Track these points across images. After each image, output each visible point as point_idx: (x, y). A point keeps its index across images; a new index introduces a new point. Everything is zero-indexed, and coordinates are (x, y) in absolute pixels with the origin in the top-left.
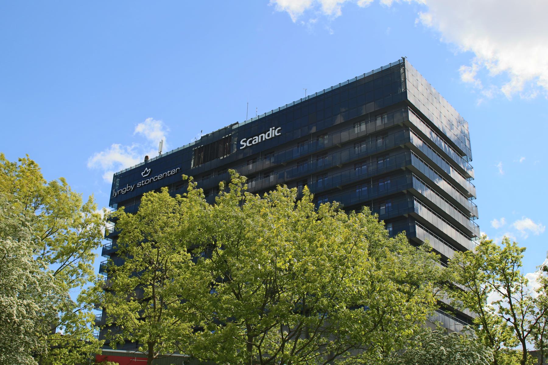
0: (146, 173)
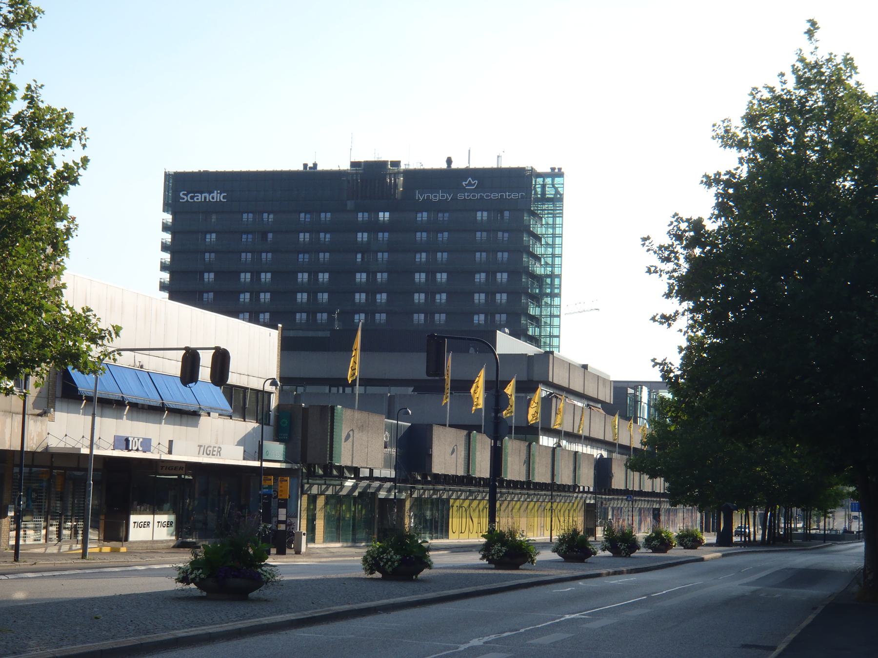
0: (470, 184)
